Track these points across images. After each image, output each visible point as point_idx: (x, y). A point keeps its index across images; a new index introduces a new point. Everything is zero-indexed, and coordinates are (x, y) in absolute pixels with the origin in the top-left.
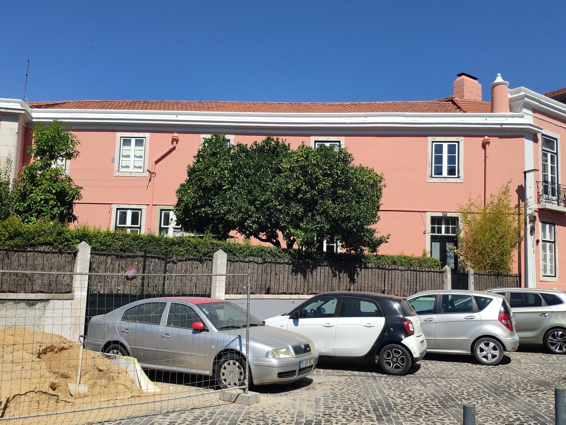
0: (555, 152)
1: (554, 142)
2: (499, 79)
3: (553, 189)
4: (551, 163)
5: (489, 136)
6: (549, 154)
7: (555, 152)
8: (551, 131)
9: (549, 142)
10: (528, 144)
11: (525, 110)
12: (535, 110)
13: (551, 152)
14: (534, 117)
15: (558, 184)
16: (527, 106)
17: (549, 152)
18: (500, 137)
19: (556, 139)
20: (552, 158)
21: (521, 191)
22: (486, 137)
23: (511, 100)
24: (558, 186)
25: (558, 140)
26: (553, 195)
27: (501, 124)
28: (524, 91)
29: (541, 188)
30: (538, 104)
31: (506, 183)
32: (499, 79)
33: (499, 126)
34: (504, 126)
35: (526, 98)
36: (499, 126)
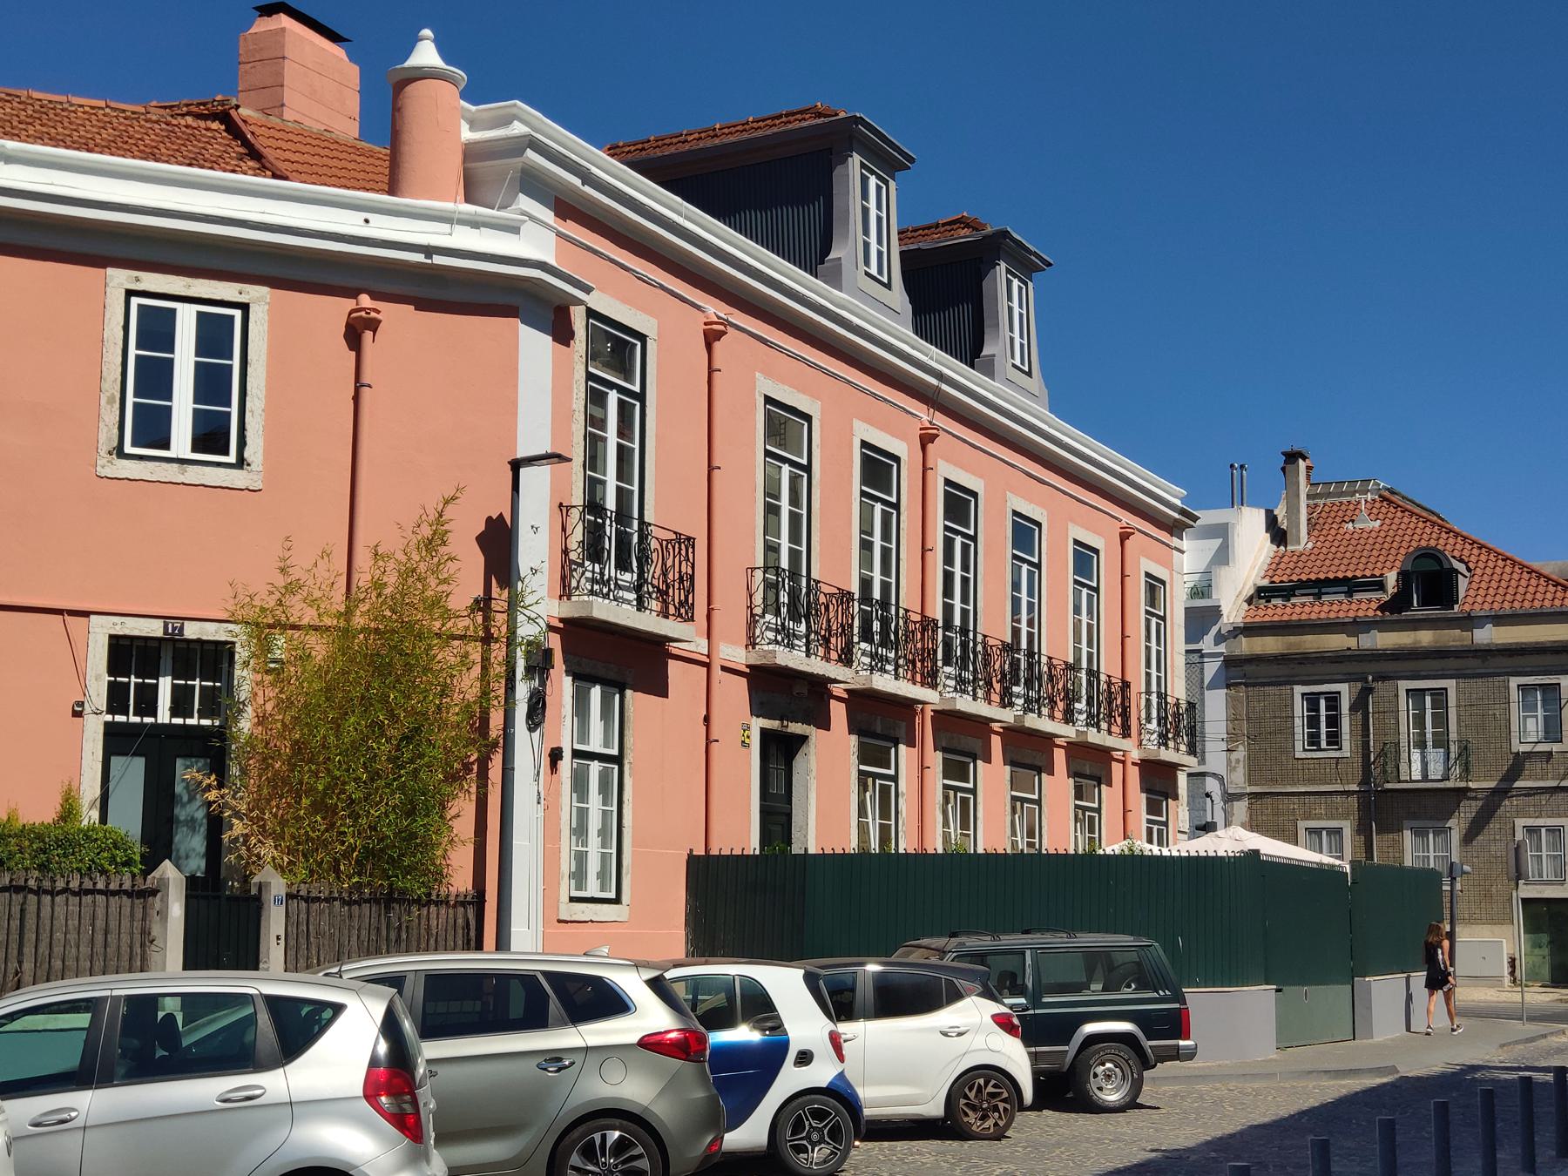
2: (426, 55)
6: (613, 397)
8: (625, 301)
11: (525, 202)
12: (567, 208)
13: (621, 390)
14: (559, 234)
16: (533, 184)
20: (624, 410)
24: (640, 530)
25: (649, 342)
26: (623, 565)
29: (577, 535)
30: (577, 182)
32: (426, 55)
35: (530, 153)
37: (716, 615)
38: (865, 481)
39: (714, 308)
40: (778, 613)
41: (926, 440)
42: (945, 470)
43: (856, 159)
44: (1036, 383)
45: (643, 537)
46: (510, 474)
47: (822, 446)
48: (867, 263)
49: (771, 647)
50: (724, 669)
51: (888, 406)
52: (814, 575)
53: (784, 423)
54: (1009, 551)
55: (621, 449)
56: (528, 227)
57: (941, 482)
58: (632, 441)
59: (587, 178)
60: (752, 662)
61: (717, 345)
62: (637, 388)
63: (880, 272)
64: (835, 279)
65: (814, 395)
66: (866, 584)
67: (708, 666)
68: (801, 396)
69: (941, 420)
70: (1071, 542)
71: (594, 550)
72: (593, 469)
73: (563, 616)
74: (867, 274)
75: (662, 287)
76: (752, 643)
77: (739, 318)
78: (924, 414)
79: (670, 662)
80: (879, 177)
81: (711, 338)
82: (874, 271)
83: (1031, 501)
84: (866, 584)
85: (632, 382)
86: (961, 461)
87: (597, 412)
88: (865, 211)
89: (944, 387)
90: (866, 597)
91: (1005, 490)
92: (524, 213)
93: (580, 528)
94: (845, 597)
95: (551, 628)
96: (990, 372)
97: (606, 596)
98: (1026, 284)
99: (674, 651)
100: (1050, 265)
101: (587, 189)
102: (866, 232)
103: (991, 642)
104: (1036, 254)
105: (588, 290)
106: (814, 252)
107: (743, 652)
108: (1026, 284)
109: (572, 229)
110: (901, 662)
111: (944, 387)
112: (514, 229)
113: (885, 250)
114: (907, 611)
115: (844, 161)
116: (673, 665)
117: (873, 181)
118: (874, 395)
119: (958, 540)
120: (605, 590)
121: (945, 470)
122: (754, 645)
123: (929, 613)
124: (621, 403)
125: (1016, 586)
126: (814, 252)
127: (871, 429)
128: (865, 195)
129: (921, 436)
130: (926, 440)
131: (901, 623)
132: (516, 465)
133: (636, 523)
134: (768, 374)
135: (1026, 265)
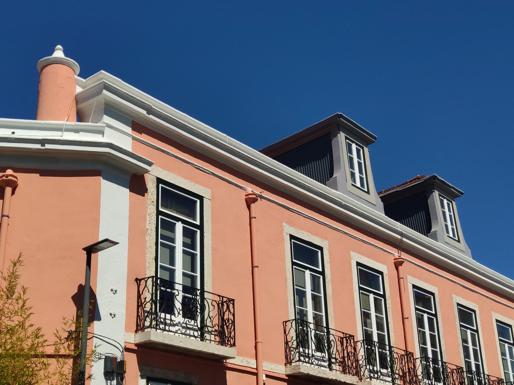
0: (198, 223)
1: (429, 299)
2: (59, 53)
3: (383, 357)
4: (430, 330)
5: (15, 170)
6: (179, 227)
7: (198, 223)
8: (186, 178)
9: (178, 201)
10: (114, 197)
11: (107, 119)
12: (139, 126)
13: (374, 293)
14: (134, 138)
15: (390, 347)
16: (111, 110)
17: (178, 220)
18: (44, 173)
19: (201, 198)
20: (430, 321)
21: (86, 303)
22: (9, 172)
23: (78, 100)
24: (442, 366)
25: (205, 201)
26: (383, 365)
27: (43, 142)
28: (105, 76)
29: (292, 334)
30: (144, 112)
31: (7, 269)
32: (59, 53)
33: (38, 146)
34: (48, 146)
35: (105, 92)
36: (38, 146)
37: (259, 345)
38: (461, 320)
39: (251, 188)
40: (429, 378)
41: (398, 264)
42: (411, 280)
43: (342, 136)
44: (463, 245)
45: (391, 352)
46: (85, 256)
47: (331, 262)
48: (448, 232)
49: (298, 363)
50: (267, 376)
51: (372, 247)
52: (486, 372)
53: (423, 298)
54: (457, 323)
55: (431, 335)
56: (107, 130)
57: (410, 287)
58: (382, 314)
59: (150, 111)
60: (289, 373)
61: (253, 206)
62: (434, 312)
63: (454, 235)
64: (435, 237)
65: (323, 238)
66: (468, 364)
67: (256, 374)
68: (315, 237)
69: (405, 256)
70: (494, 322)
71: (303, 341)
72: (366, 326)
73: (136, 342)
74: (448, 236)
75: (213, 174)
76: (288, 362)
77: (266, 194)
78: (396, 253)
79: (229, 373)
80: (447, 200)
81: (250, 201)
82: (451, 235)
83: (468, 300)
84: (468, 364)
85: (195, 219)
86: (417, 276)
87: (465, 338)
88: (444, 213)
89: (404, 239)
90: (469, 371)
91: (450, 295)
92: (105, 123)
93: (420, 367)
94: (459, 370)
95: (127, 350)
96: (436, 239)
97: (377, 378)
98: (451, 202)
99: (229, 365)
100: (462, 194)
101: (151, 116)
102: (445, 220)
103: (492, 378)
104: (453, 188)
105: (150, 164)
106: (326, 175)
107: (283, 367)
108: (451, 202)
109: (144, 137)
110: (333, 360)
111: (404, 239)
112: (102, 133)
113: (455, 227)
114: (488, 376)
115: (336, 135)
116: (229, 373)
117: (445, 201)
118: (363, 241)
119: (426, 316)
120: (376, 376)
121: (411, 280)
122: (291, 363)
123: (410, 350)
124: (428, 318)
125: (465, 341)
126: (326, 175)
127: (362, 257)
128: (443, 206)
129: (395, 263)
130: (398, 264)
131: (487, 381)
132: (91, 250)
133: (440, 363)
134: (291, 224)
135: (450, 194)
